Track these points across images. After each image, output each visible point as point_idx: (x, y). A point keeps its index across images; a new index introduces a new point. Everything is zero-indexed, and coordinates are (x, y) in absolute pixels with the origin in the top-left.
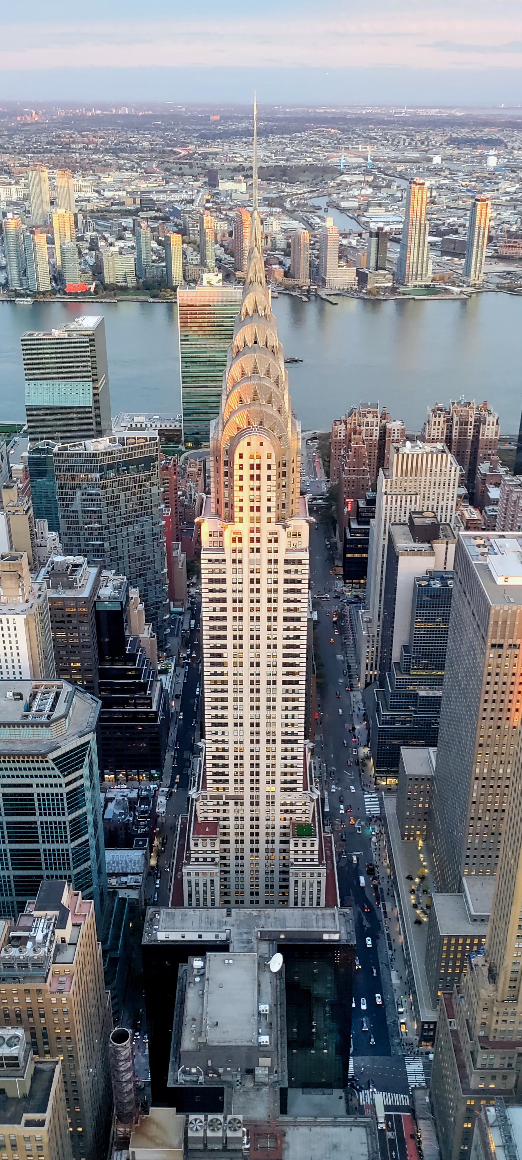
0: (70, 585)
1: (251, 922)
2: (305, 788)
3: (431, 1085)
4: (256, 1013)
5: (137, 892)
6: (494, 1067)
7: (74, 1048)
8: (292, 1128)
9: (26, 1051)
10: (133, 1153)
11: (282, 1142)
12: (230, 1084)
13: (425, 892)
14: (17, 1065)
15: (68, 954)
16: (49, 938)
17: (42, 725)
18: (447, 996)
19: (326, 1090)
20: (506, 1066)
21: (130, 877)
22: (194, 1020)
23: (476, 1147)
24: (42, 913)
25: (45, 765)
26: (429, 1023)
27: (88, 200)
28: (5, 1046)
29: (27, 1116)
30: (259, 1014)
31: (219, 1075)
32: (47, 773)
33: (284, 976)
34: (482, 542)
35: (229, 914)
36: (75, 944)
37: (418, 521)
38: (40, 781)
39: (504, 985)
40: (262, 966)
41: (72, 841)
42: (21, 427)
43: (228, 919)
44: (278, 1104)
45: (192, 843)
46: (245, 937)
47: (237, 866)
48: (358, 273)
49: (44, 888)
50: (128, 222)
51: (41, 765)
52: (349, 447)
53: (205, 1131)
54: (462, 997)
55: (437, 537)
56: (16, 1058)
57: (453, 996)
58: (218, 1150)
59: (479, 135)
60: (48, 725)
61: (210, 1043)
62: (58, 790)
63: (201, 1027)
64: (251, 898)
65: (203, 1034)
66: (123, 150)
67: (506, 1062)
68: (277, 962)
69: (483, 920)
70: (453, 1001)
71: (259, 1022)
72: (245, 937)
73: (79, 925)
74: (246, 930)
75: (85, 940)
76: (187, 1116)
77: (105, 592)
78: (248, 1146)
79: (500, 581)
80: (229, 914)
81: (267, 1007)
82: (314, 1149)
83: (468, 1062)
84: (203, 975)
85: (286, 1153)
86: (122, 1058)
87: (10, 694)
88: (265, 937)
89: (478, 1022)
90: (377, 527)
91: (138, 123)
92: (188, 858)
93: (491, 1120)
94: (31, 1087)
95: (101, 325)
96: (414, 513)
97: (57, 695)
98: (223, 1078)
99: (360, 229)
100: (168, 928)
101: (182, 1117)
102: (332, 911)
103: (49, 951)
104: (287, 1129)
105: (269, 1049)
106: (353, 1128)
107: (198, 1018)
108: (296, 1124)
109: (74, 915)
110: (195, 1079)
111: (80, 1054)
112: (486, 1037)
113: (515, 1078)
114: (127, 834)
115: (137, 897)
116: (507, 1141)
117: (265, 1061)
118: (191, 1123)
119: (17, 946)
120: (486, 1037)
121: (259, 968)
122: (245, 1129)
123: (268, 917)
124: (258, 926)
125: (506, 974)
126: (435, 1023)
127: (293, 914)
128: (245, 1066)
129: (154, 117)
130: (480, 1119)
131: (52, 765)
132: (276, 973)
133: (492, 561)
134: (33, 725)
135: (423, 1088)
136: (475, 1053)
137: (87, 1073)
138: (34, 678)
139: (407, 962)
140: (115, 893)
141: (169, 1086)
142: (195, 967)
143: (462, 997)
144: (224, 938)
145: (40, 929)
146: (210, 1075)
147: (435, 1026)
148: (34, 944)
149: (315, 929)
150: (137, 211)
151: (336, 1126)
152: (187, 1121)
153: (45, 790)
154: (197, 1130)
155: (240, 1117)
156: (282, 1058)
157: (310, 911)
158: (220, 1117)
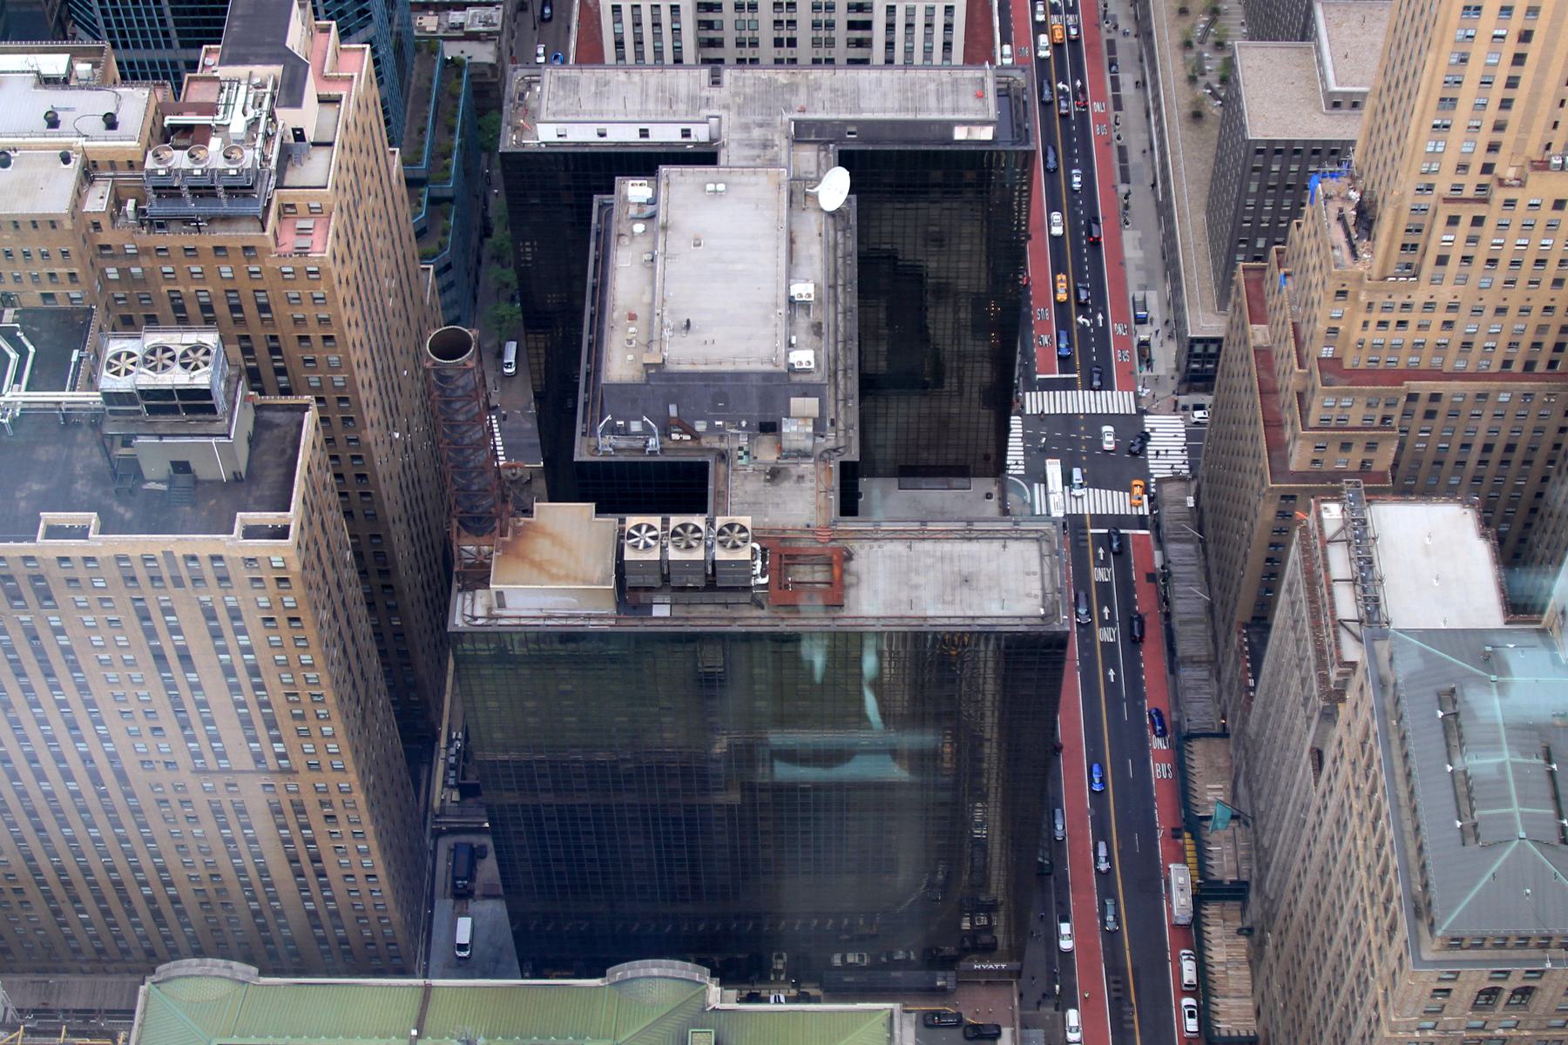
1: (772, 98)
3: (1202, 472)
4: (783, 301)
5: (491, 47)
6: (1350, 424)
7: (351, 382)
8: (867, 544)
9: (228, 382)
10: (500, 594)
11: (843, 571)
12: (723, 456)
13: (1219, 46)
14: (212, 409)
15: (317, 169)
16: (261, 129)
18: (1252, 275)
19: (956, 482)
20: (1377, 423)
21: (471, 11)
22: (632, 317)
23: (1291, 585)
24: (240, 71)
26: (1206, 341)
28: (177, 368)
29: (243, 518)
30: (791, 302)
31: (696, 437)
33: (853, 222)
35: (716, 82)
36: (330, 144)
39: (1391, 240)
40: (799, 197)
43: (714, 92)
44: (834, 498)
46: (757, 133)
49: (239, 12)
53: (663, 549)
54: (1286, 275)
56: (206, 394)
57: (1268, 274)
58: (695, 589)
61: (672, 367)
63: (650, 332)
64: (775, 53)
65: (655, 347)
67: (1378, 413)
68: (835, 188)
69: (1355, 105)
70: (1267, 287)
71: (791, 320)
72: (757, 133)
73: (336, 101)
74: (759, 118)
75: (355, 137)
76: (622, 521)
78: (765, 580)
80: (716, 82)
81: (810, 288)
82: (916, 587)
83: (1291, 415)
84: (652, 217)
85: (852, 593)
86: (460, 392)
88: (804, 133)
89: (1321, 327)
93: (1330, 529)
94: (250, 461)
98: (704, 442)
100: (564, 112)
101: (611, 521)
102: (979, 74)
103: (265, 158)
104: (855, 546)
105: (817, 378)
106: (1010, 543)
107: (641, 313)
108: (873, 537)
110: (640, 444)
111: (364, 395)
112: (1337, 360)
113: (1394, 449)
115: (491, 59)
116: (1361, 569)
117: (806, 406)
118: (631, 536)
119: (184, 148)
120: (1337, 360)
121: (791, 201)
122: (757, 546)
123: (815, 87)
124: (788, 109)
125: (1398, 211)
126: (1217, 341)
127: (879, 82)
128: (757, 415)
130: (1305, 530)
132: (832, 214)
135: (1182, 479)
136: (1308, 395)
137: (386, 444)
139: (1164, 210)
140: (434, 51)
141: (576, 458)
142: (632, 199)
143: (1286, 275)
144: (704, 138)
145: (239, 107)
146: (675, 436)
147: (1219, 349)
149: (935, 116)
151: (970, 539)
152: (623, 530)
154: (647, 546)
155: (746, 521)
156: (845, 400)
157: (923, 74)
158: (698, 520)
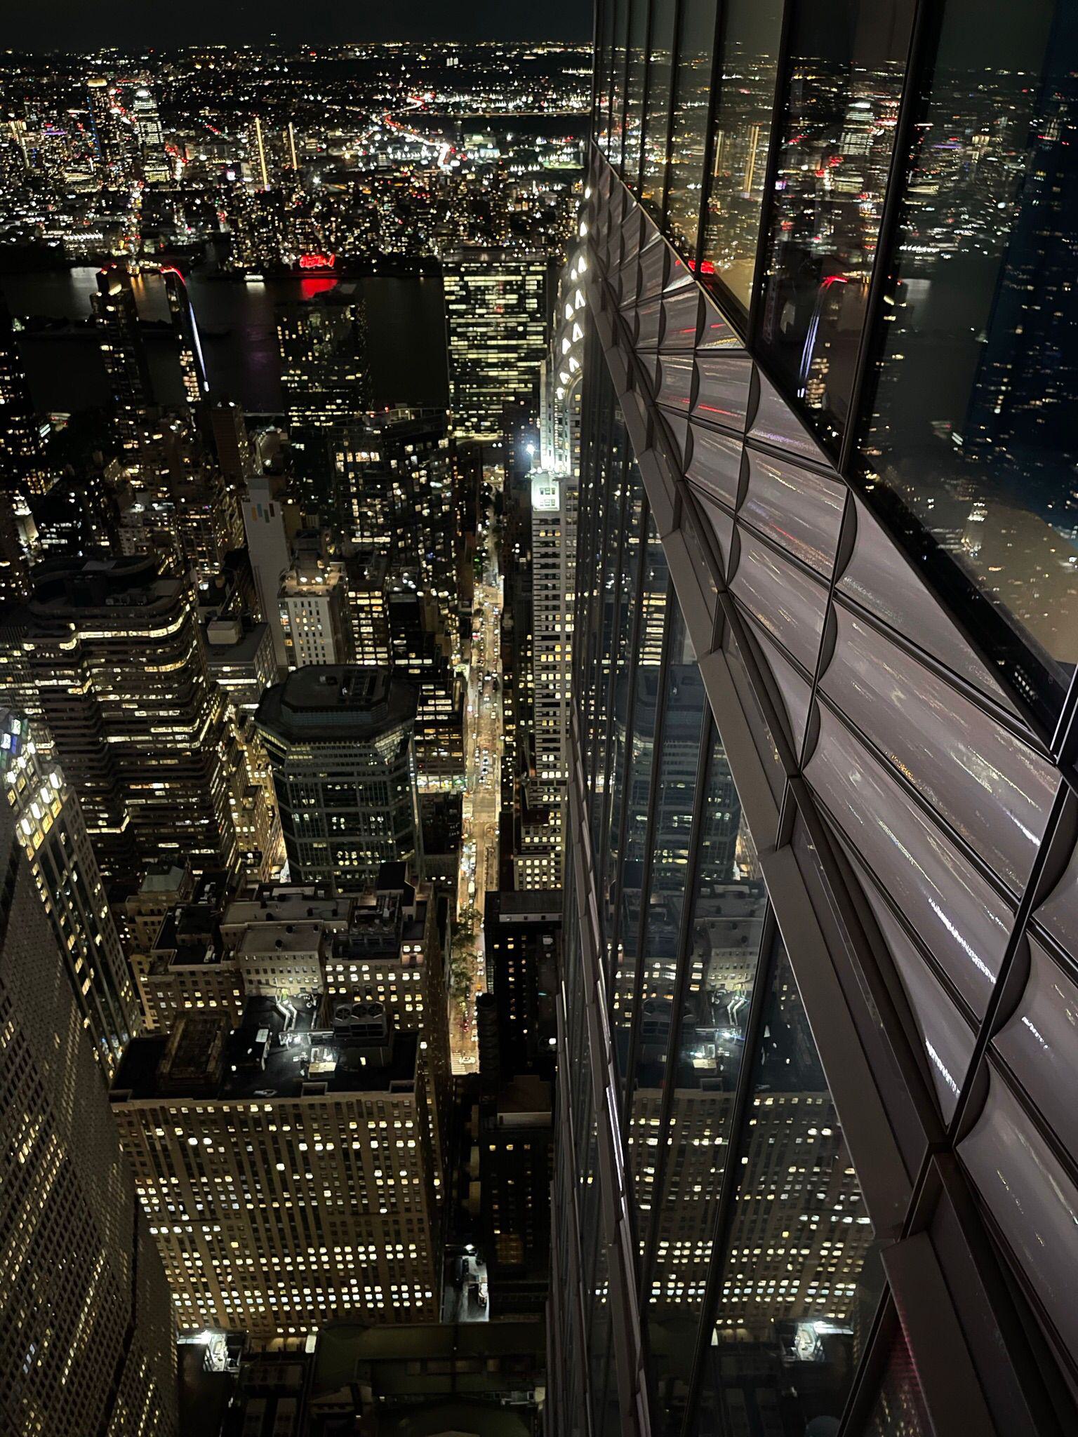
17: (361, 709)
60: (367, 709)
87: (323, 679)
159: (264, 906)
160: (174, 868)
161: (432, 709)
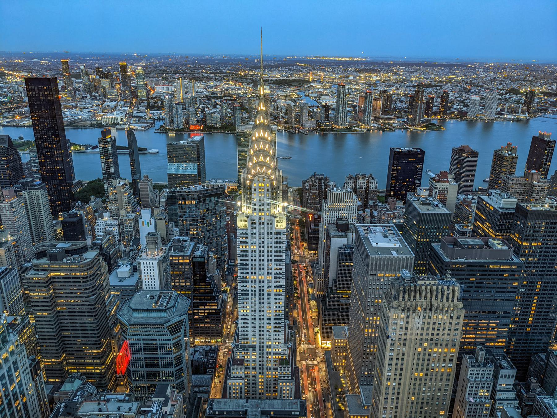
0: (182, 250)
2: (285, 342)
17: (162, 310)
24: (157, 399)
25: (163, 330)
27: (202, 92)
32: (164, 333)
34: (366, 228)
35: (247, 402)
37: (340, 222)
38: (160, 337)
41: (175, 367)
42: (166, 185)
45: (231, 368)
47: (253, 380)
48: (317, 122)
50: (218, 101)
51: (161, 330)
52: (310, 192)
55: (348, 229)
59: (369, 68)
60: (165, 311)
62: (169, 342)
66: (218, 73)
72: (254, 413)
73: (174, 405)
77: (198, 253)
79: (374, 245)
80: (247, 402)
87: (148, 296)
90: (323, 226)
91: (225, 62)
92: (230, 376)
95: (202, 139)
96: (338, 219)
97: (170, 297)
99: (318, 104)
109: (172, 401)
114: (204, 367)
129: (231, 60)
131: (166, 329)
133: (371, 236)
134: (158, 310)
138: (161, 288)
148: (152, 414)
149: (288, 409)
150: (222, 97)
153: (163, 342)
159: (99, 404)
160: (77, 380)
161: (209, 307)
